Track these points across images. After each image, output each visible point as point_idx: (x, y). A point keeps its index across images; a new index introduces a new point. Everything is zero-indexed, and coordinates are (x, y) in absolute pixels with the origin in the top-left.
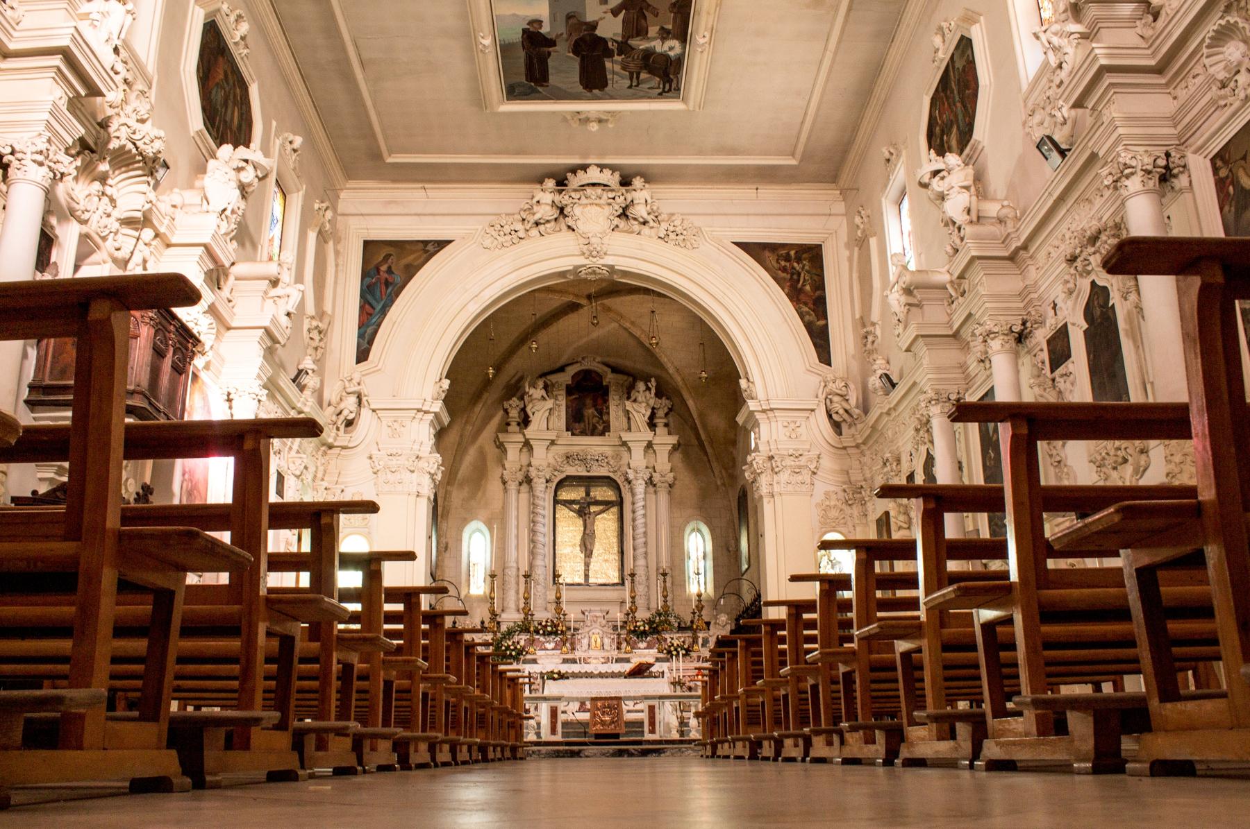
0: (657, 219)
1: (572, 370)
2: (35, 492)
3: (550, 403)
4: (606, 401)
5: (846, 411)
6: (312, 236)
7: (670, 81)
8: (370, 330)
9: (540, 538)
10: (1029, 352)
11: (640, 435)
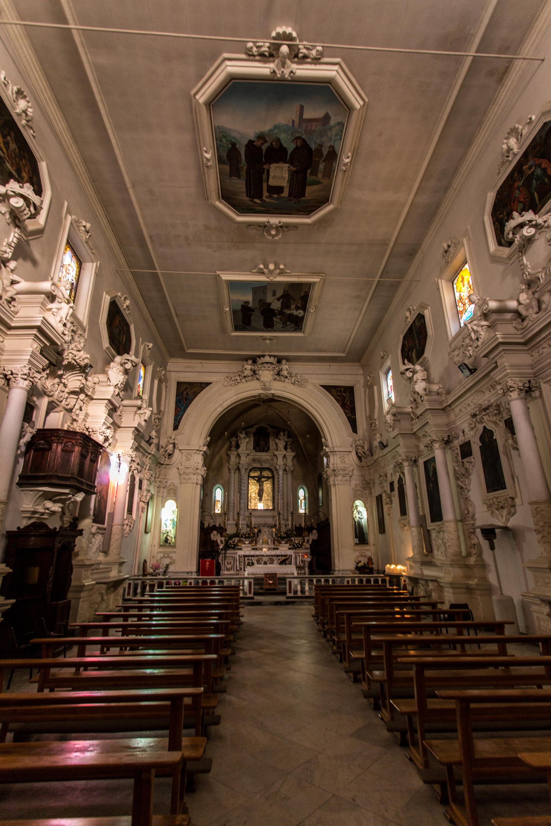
0: (291, 376)
1: (256, 427)
2: (18, 528)
3: (247, 440)
4: (268, 439)
5: (364, 452)
6: (156, 382)
7: (298, 326)
8: (179, 417)
9: (243, 492)
10: (450, 448)
11: (281, 453)
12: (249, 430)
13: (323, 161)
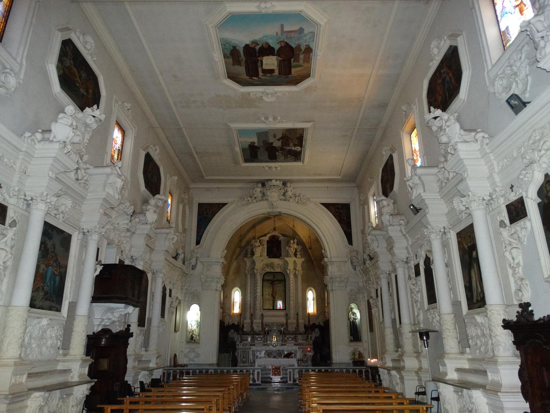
1: (268, 236)
2: (94, 333)
12: (262, 238)
13: (303, 54)
